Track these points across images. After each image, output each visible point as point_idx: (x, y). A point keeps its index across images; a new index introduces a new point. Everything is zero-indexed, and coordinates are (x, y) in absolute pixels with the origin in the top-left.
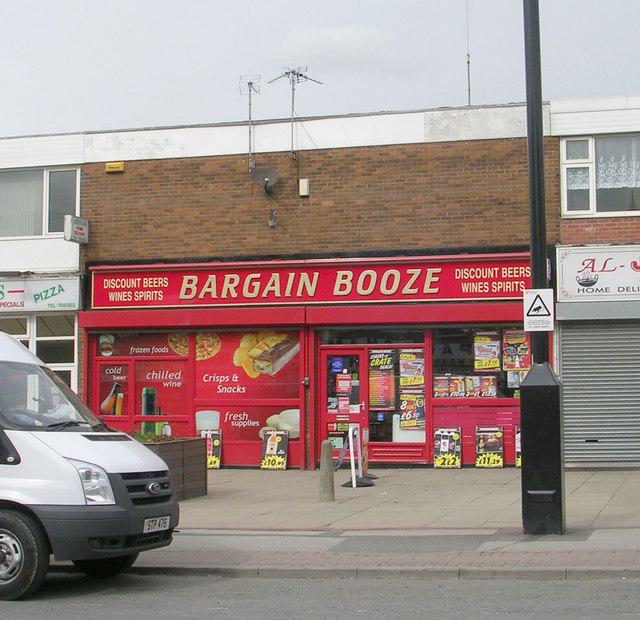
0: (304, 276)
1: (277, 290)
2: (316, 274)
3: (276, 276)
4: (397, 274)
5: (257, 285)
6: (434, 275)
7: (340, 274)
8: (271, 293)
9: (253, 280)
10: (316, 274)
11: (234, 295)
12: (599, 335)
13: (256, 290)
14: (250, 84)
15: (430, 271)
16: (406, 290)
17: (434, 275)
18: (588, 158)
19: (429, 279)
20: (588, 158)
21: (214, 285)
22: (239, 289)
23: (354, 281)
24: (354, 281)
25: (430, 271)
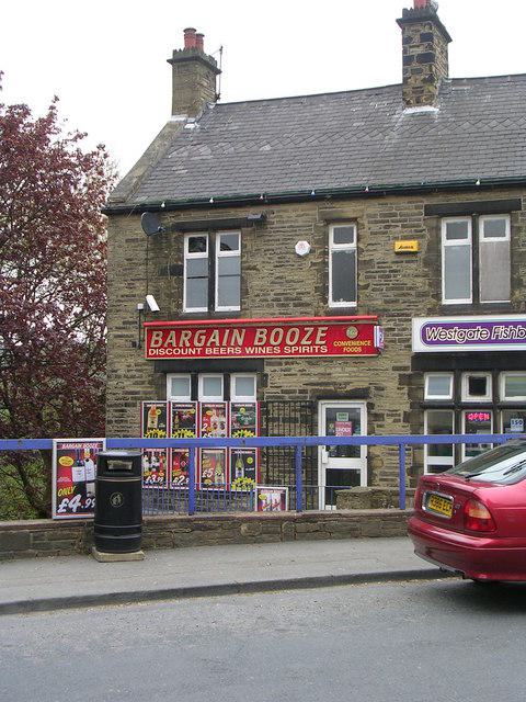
0: (236, 331)
1: (217, 341)
2: (244, 330)
3: (216, 332)
4: (281, 330)
5: (203, 338)
6: (323, 332)
7: (155, 333)
8: (170, 345)
9: (201, 334)
10: (244, 330)
11: (188, 344)
12: (257, 597)
13: (160, 342)
14: (57, 99)
15: (321, 329)
16: (304, 342)
17: (323, 332)
18: (447, 239)
19: (320, 334)
20: (447, 239)
21: (174, 338)
22: (191, 341)
23: (268, 336)
24: (268, 336)
25: (321, 329)
